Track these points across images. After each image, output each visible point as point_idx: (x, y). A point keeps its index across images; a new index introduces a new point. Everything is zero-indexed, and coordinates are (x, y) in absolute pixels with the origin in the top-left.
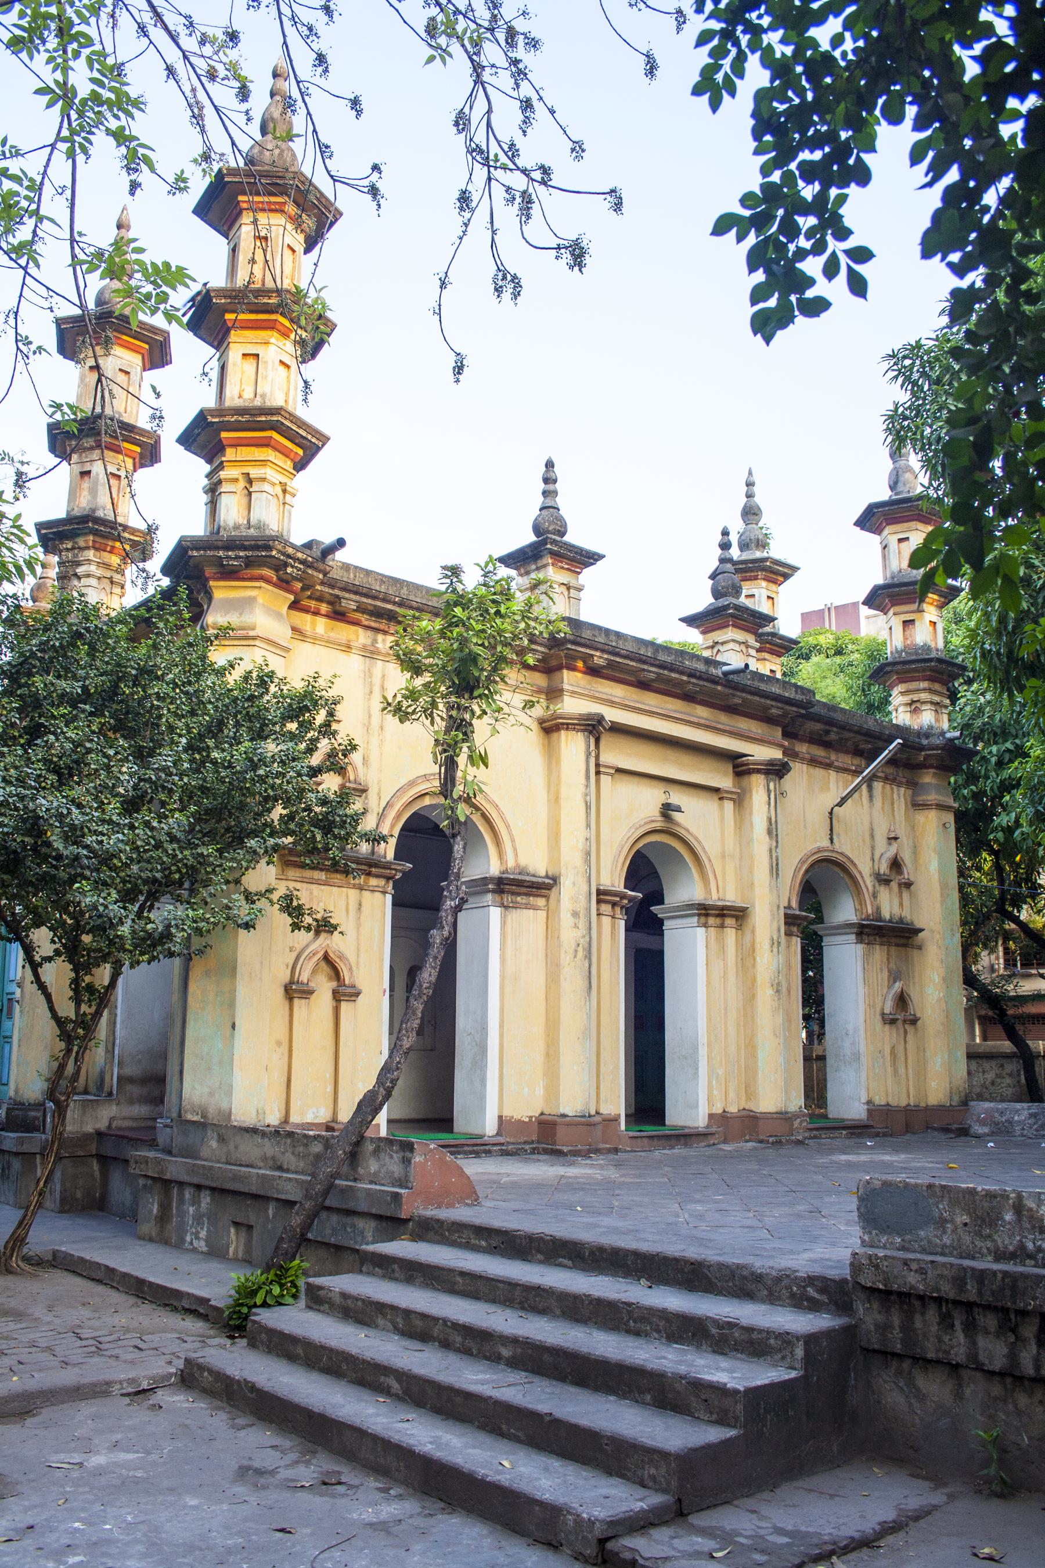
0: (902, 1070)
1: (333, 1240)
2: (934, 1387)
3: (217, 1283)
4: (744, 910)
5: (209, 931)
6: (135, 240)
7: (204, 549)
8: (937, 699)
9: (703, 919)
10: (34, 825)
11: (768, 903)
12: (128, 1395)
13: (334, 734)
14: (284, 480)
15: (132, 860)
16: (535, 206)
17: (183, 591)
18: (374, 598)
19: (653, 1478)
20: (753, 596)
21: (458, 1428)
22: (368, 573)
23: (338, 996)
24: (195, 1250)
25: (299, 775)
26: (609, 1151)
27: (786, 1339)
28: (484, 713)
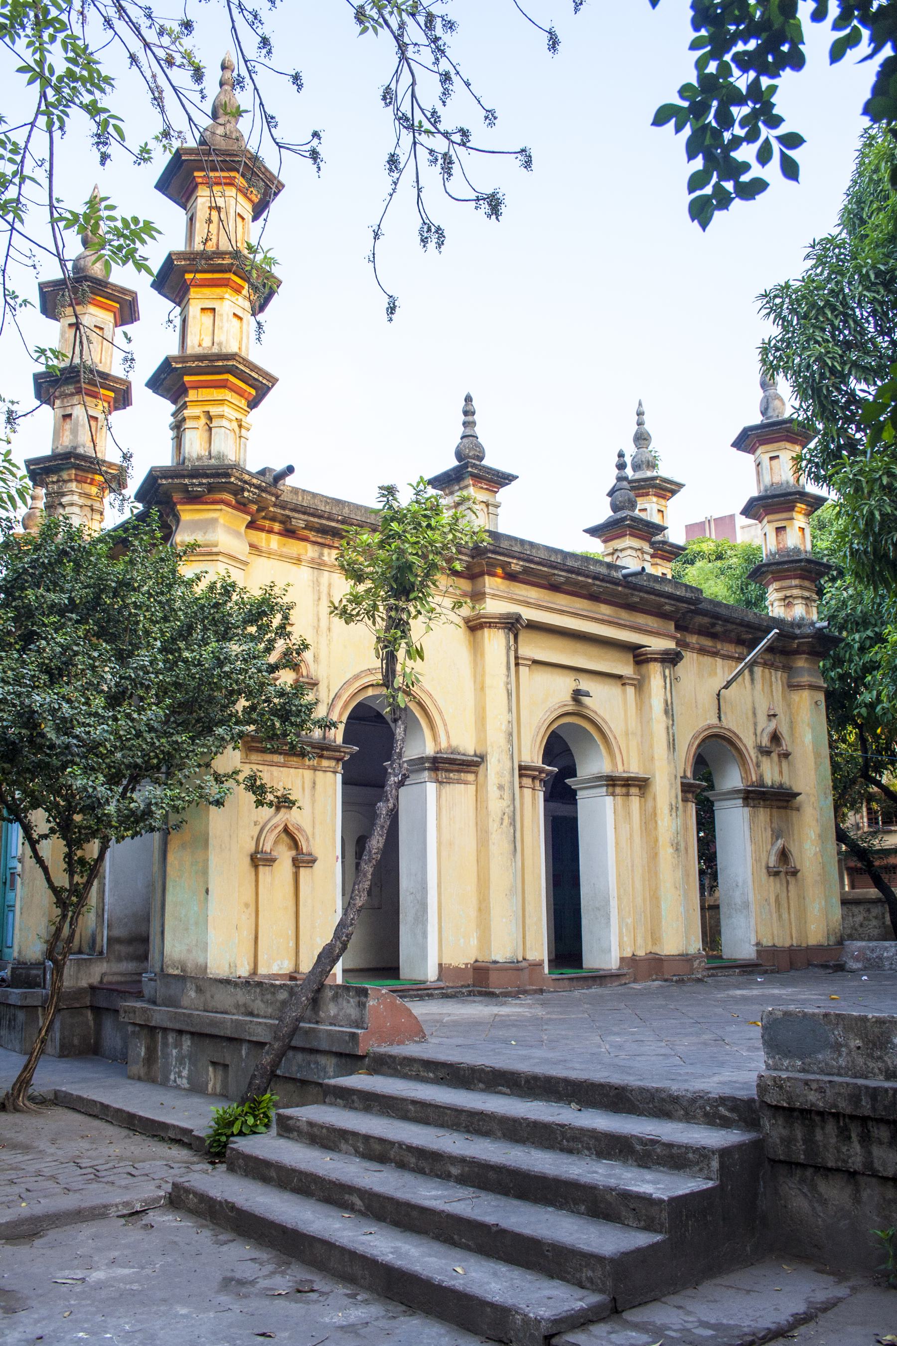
0: (785, 916)
1: (298, 1076)
2: (835, 1192)
3: (199, 1116)
4: (646, 780)
5: (184, 808)
6: (107, 198)
7: (172, 478)
8: (807, 594)
9: (611, 789)
10: (29, 719)
11: (666, 774)
12: (123, 1216)
13: (289, 635)
14: (239, 416)
15: (116, 747)
16: (456, 169)
17: (154, 511)
18: (320, 517)
19: (591, 1280)
20: (645, 510)
21: (415, 1239)
22: (314, 495)
23: (297, 863)
24: (178, 1087)
25: (260, 671)
26: (536, 992)
27: (703, 1153)
28: (419, 612)
